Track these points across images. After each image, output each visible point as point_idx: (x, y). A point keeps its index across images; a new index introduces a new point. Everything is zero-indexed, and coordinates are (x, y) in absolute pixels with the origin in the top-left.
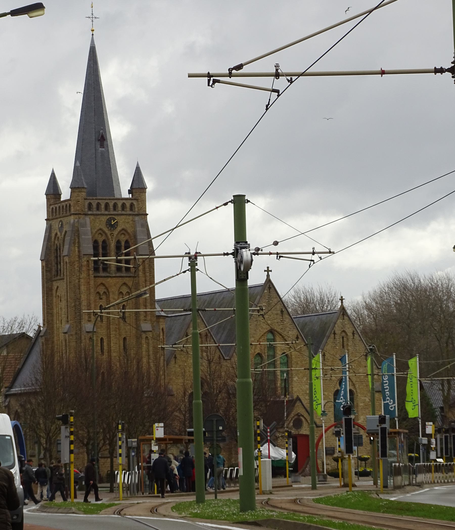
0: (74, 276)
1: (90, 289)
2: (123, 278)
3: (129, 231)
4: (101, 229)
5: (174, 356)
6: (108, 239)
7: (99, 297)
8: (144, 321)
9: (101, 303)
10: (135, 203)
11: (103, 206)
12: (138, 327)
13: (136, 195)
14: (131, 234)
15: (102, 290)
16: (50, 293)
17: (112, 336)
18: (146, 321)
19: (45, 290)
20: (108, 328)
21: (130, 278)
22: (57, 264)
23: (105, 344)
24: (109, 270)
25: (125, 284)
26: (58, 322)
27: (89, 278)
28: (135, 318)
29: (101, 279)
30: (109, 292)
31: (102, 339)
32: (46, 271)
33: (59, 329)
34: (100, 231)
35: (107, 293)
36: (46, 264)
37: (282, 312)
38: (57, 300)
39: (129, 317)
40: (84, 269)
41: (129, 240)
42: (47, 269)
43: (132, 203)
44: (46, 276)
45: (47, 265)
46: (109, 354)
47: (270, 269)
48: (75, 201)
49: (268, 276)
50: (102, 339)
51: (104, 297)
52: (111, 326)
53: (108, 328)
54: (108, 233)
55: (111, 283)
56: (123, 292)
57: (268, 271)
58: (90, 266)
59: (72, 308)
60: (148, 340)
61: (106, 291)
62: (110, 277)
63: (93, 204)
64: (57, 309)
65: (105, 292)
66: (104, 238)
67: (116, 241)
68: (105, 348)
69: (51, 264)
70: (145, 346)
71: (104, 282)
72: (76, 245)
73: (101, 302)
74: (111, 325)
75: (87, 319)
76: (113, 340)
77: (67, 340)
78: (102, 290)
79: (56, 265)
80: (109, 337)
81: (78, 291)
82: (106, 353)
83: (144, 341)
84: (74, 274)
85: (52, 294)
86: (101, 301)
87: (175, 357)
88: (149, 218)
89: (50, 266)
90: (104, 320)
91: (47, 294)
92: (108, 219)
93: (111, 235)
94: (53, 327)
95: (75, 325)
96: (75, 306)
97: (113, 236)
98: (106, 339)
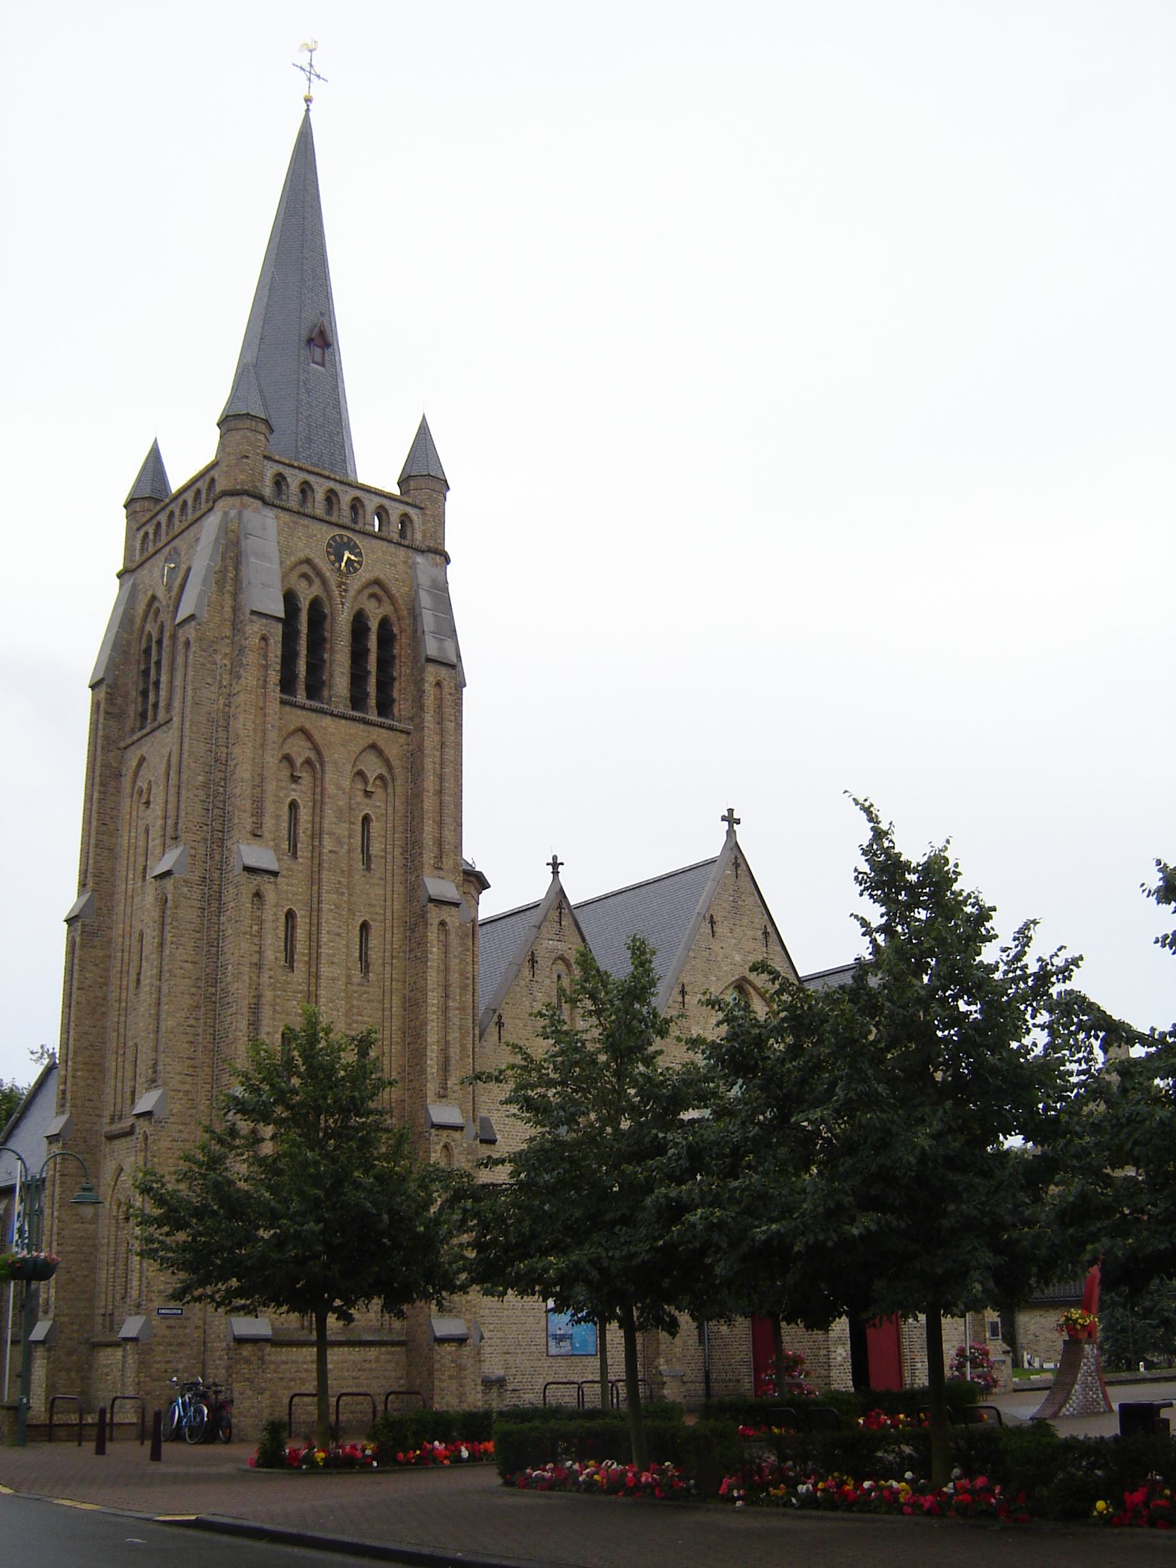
0: (212, 689)
1: (264, 732)
2: (371, 728)
3: (394, 590)
4: (308, 561)
5: (495, 1019)
6: (330, 597)
7: (288, 774)
8: (435, 872)
9: (294, 795)
10: (414, 517)
11: (320, 496)
12: (413, 888)
13: (420, 497)
14: (400, 601)
15: (300, 750)
16: (113, 784)
17: (325, 906)
18: (441, 873)
19: (98, 773)
20: (315, 880)
21: (390, 733)
22: (144, 694)
23: (301, 934)
24: (326, 693)
25: (373, 747)
26: (131, 876)
27: (265, 695)
28: (404, 862)
29: (299, 712)
30: (322, 764)
31: (290, 915)
32: (107, 713)
33: (133, 897)
34: (305, 568)
35: (318, 766)
36: (107, 693)
37: (766, 934)
38: (135, 807)
39: (382, 857)
40: (251, 658)
41: (393, 618)
42: (110, 710)
43: (406, 515)
44: (104, 729)
45: (110, 698)
46: (313, 970)
47: (735, 816)
48: (232, 457)
49: (731, 833)
50: (290, 915)
51: (305, 775)
52: (325, 875)
53: (315, 880)
54: (333, 579)
55: (333, 734)
56: (366, 771)
57: (731, 819)
58: (271, 655)
59: (197, 792)
60: (447, 933)
61: (312, 756)
62: (332, 714)
63: (289, 480)
64: (133, 834)
65: (308, 762)
66: (316, 590)
67: (354, 611)
68: (301, 947)
69: (125, 697)
70: (435, 950)
71: (308, 726)
72: (229, 588)
73: (293, 790)
74: (325, 872)
75: (249, 828)
76: (329, 922)
77: (170, 897)
78: (300, 750)
79: (140, 699)
80: (315, 911)
81: (222, 734)
82: (300, 967)
83: (433, 934)
84: (209, 681)
85: (118, 790)
86: (294, 786)
87: (500, 1024)
88: (455, 575)
89: (119, 701)
90: (299, 853)
91: (102, 784)
92: (334, 537)
93: (340, 584)
94: (112, 894)
95: (201, 850)
96: (205, 785)
97: (345, 591)
98: (304, 917)
